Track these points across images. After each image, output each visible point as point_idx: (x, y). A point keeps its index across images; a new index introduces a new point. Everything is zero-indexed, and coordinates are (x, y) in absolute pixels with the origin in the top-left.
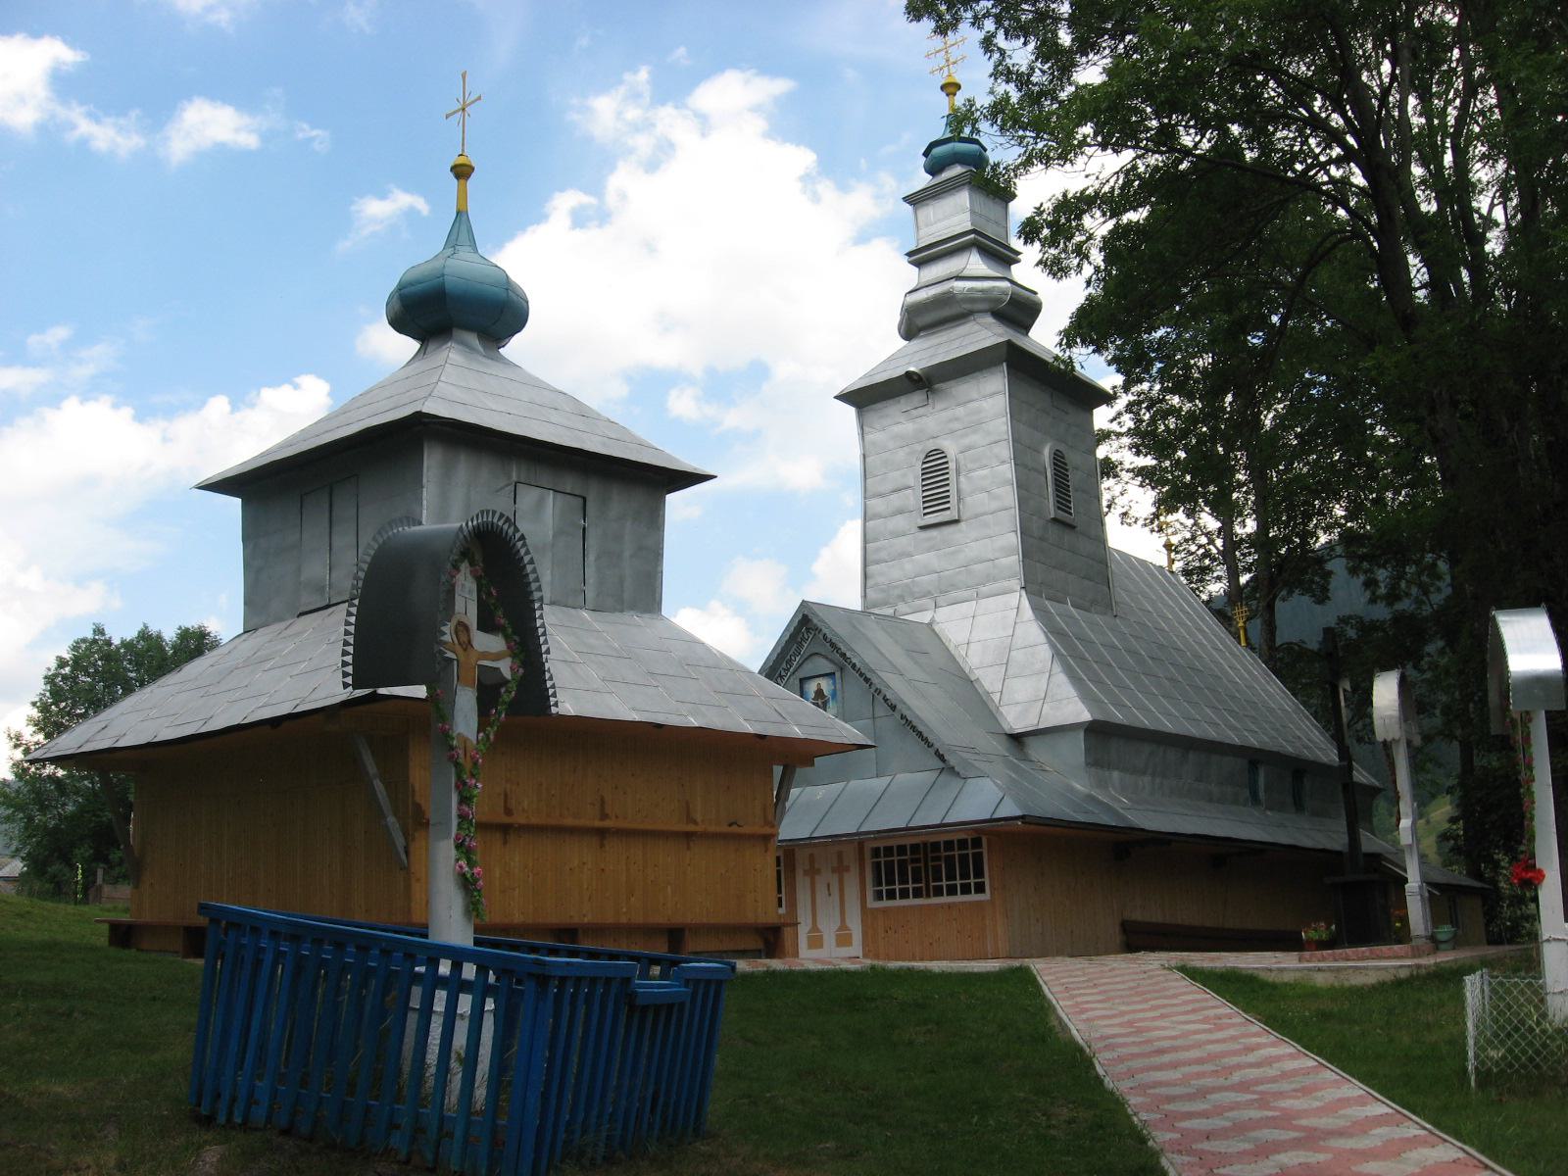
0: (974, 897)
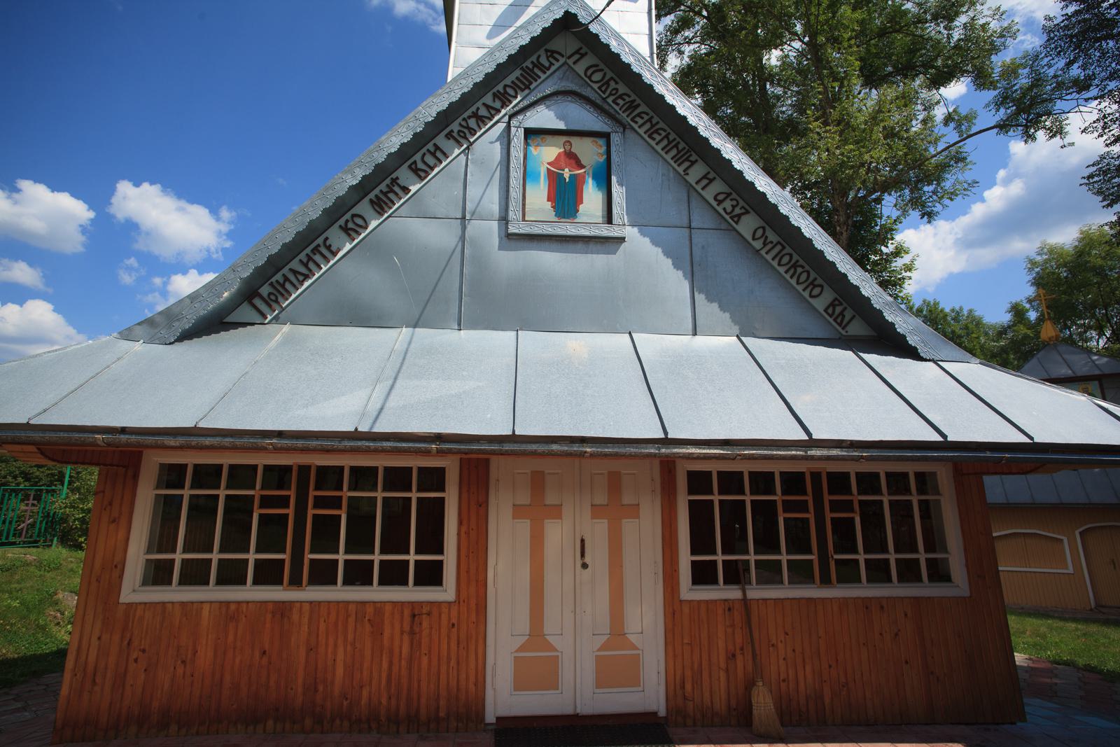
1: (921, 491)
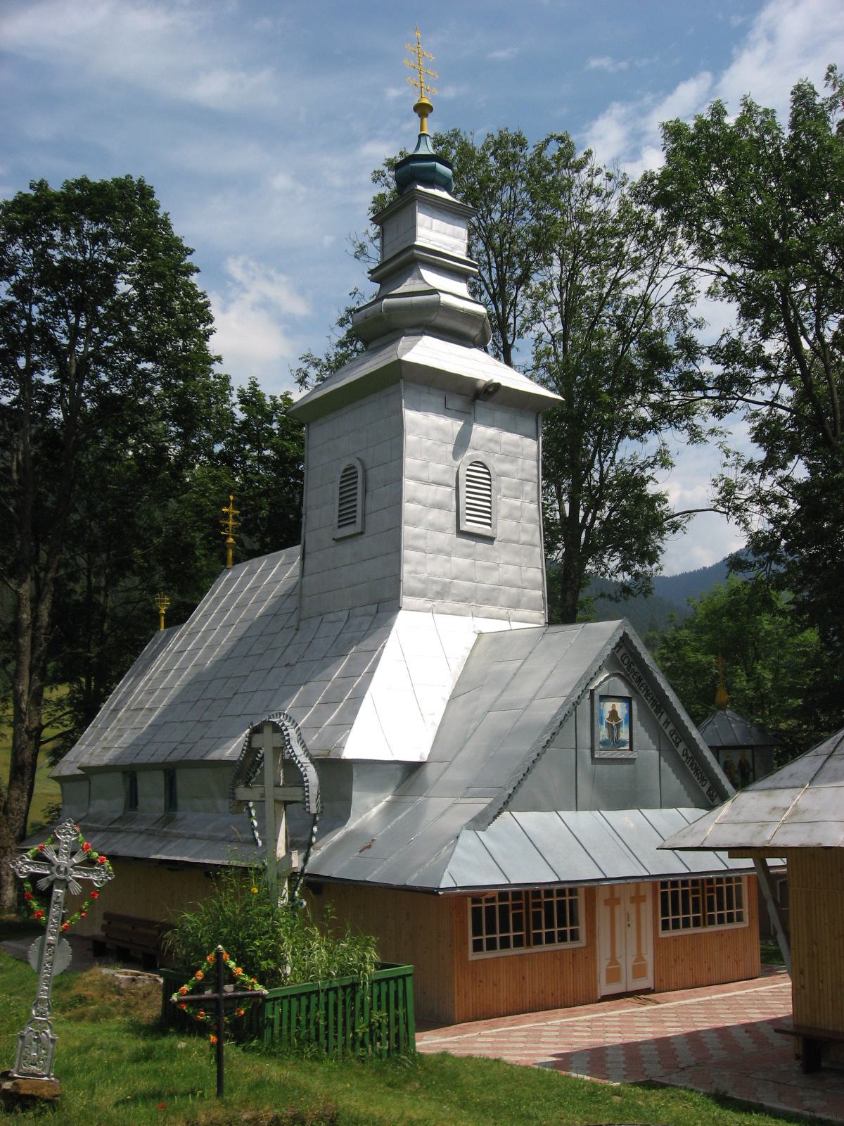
0: (569, 945)
1: (722, 883)
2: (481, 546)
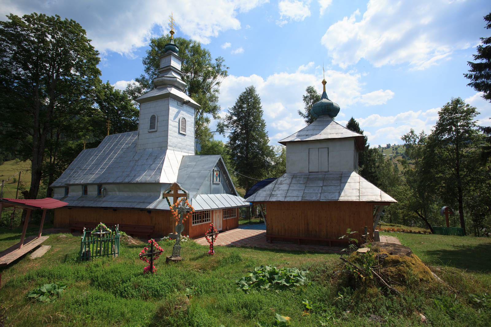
2: (183, 137)
